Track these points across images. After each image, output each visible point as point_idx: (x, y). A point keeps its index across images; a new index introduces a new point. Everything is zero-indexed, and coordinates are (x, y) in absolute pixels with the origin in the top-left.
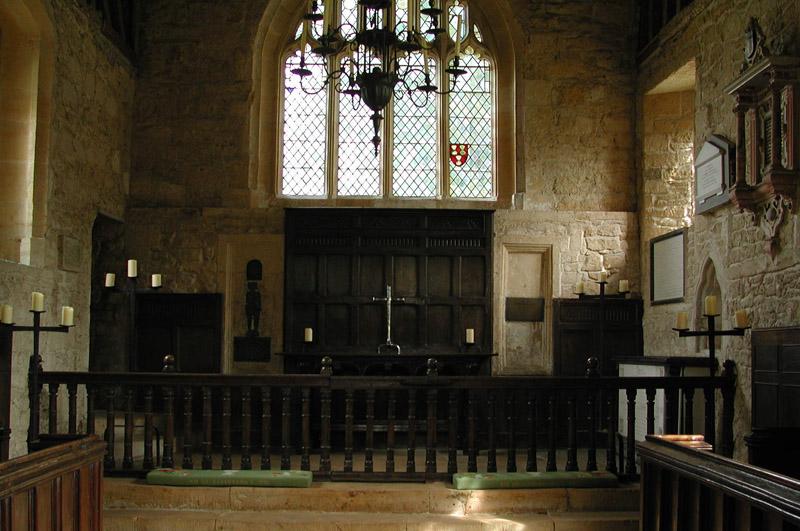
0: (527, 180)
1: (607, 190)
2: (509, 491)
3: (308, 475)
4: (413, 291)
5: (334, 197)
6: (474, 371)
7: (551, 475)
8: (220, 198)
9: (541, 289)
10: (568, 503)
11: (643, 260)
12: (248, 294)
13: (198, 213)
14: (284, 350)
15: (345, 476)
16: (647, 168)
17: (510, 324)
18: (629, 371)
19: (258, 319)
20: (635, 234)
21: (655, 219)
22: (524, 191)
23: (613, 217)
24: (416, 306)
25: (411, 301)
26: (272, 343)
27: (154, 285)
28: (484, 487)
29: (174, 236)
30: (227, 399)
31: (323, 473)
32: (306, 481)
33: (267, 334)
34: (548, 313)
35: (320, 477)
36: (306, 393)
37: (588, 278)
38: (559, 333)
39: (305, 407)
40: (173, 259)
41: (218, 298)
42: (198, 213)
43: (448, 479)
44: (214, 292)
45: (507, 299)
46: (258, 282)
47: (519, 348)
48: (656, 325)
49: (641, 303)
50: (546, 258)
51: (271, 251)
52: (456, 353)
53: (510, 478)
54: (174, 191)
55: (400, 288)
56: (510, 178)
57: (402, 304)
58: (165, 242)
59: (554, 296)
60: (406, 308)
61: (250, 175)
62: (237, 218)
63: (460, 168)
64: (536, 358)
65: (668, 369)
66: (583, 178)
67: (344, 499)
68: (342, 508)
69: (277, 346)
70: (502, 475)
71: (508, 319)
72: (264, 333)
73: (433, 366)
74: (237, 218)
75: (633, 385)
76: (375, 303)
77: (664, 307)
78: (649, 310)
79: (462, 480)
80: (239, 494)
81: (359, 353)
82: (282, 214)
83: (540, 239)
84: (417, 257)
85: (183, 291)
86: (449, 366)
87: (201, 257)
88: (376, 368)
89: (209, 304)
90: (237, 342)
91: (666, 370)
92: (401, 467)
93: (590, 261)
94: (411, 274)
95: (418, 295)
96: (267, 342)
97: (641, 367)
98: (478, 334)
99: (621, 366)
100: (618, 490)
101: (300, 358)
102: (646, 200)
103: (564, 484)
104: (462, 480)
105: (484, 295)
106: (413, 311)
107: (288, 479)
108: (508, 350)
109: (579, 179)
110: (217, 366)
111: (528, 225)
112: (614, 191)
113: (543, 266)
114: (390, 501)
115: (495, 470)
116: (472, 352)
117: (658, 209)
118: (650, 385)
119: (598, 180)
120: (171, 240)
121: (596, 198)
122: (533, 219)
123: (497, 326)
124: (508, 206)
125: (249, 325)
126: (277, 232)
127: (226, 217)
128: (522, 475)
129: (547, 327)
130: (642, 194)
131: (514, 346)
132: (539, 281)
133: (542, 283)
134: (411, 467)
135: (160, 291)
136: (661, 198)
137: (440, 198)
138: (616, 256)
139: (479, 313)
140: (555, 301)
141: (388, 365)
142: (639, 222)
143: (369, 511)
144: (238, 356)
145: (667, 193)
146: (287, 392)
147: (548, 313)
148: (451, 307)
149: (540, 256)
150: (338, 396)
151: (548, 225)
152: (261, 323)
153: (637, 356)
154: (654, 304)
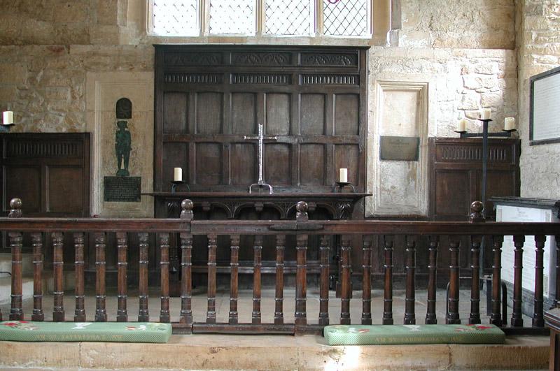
0: (403, 16)
1: (484, 27)
2: (386, 347)
3: (167, 327)
4: (285, 129)
5: (206, 34)
6: (348, 213)
7: (431, 329)
8: (88, 35)
9: (417, 128)
10: (450, 360)
11: (522, 98)
12: (118, 133)
13: (66, 50)
14: (154, 190)
15: (274, 329)
16: (527, 4)
17: (385, 164)
18: (507, 214)
19: (128, 158)
20: (515, 72)
21: (535, 56)
22: (399, 27)
23: (491, 55)
24: (289, 146)
25: (284, 139)
26: (142, 183)
27: (6, 122)
28: (364, 343)
29: (41, 73)
30: (79, 246)
31: (184, 325)
32: (163, 336)
33: (137, 174)
34: (424, 153)
35: (184, 327)
36: (165, 238)
37: (464, 117)
38: (435, 174)
39: (164, 254)
40: (42, 100)
41: (87, 136)
42: (66, 50)
43: (319, 331)
44: (82, 131)
45: (382, 138)
46: (129, 121)
47: (393, 187)
48: (535, 165)
49: (518, 143)
50: (422, 96)
51: (141, 88)
52: (329, 193)
53: (387, 333)
54: (40, 28)
55: (272, 126)
56: (385, 16)
57: (275, 143)
58: (32, 80)
59: (429, 136)
60: (277, 147)
61: (119, 12)
62: (106, 55)
63: (334, 5)
64: (410, 198)
65: (556, 213)
66: (461, 15)
67: (205, 356)
68: (203, 365)
69: (147, 186)
70: (377, 329)
71: (383, 158)
72: (134, 172)
73: (303, 210)
74: (106, 55)
75: (520, 231)
76: (246, 142)
77: (546, 147)
78: (526, 149)
79: (336, 333)
80: (91, 351)
81: (229, 193)
82: (152, 51)
83: (417, 78)
84: (289, 95)
85: (52, 130)
86: (322, 209)
87: (69, 96)
88: (246, 210)
89: (78, 142)
90: (108, 183)
91: (553, 214)
92: (245, 316)
93: (467, 99)
94: (284, 112)
95: (290, 134)
96: (137, 183)
97: (522, 209)
98: (351, 175)
99: (499, 207)
100: (505, 346)
101: (166, 201)
102: (526, 37)
103: (448, 340)
104: (336, 333)
105: (358, 134)
106: (285, 150)
107: (144, 334)
108: (382, 189)
109: (456, 15)
110: (85, 208)
111: (404, 62)
112: (493, 28)
113: (418, 104)
114: (255, 357)
115: (391, 323)
116: (345, 192)
117: (539, 47)
118: (539, 231)
119: (476, 17)
120: (38, 79)
121: (473, 35)
122: (409, 56)
123: (372, 165)
124: (383, 43)
125: (119, 165)
126: (146, 69)
127: (94, 54)
128: (399, 329)
129: (422, 166)
130: (522, 31)
131: (388, 186)
132: (414, 121)
133: (417, 122)
134: (257, 319)
135: (13, 130)
136: (542, 35)
137: (313, 35)
138: (493, 95)
139: (352, 151)
140: (431, 140)
141: (259, 206)
142: (517, 60)
143: (233, 368)
144: (108, 197)
145: (548, 29)
146: (144, 238)
147: (424, 153)
148: (324, 145)
149: (415, 94)
150: (200, 244)
151: (424, 63)
152: (131, 162)
153: (513, 195)
154: (533, 144)
